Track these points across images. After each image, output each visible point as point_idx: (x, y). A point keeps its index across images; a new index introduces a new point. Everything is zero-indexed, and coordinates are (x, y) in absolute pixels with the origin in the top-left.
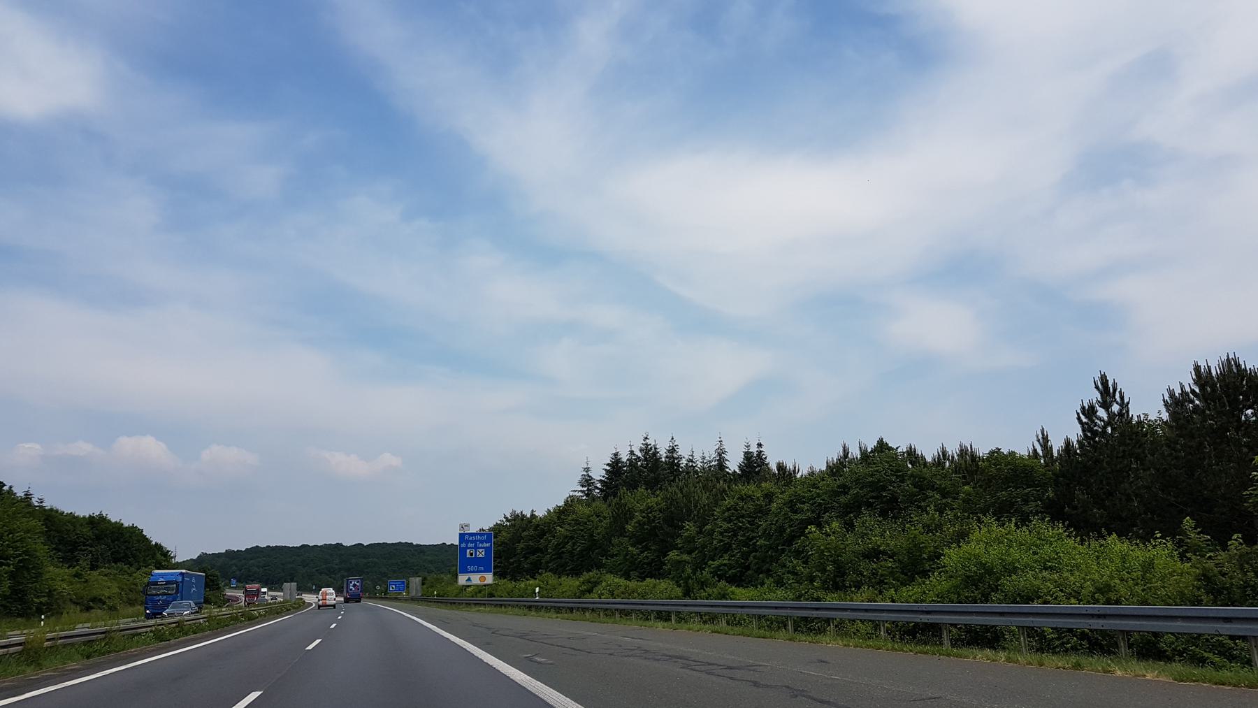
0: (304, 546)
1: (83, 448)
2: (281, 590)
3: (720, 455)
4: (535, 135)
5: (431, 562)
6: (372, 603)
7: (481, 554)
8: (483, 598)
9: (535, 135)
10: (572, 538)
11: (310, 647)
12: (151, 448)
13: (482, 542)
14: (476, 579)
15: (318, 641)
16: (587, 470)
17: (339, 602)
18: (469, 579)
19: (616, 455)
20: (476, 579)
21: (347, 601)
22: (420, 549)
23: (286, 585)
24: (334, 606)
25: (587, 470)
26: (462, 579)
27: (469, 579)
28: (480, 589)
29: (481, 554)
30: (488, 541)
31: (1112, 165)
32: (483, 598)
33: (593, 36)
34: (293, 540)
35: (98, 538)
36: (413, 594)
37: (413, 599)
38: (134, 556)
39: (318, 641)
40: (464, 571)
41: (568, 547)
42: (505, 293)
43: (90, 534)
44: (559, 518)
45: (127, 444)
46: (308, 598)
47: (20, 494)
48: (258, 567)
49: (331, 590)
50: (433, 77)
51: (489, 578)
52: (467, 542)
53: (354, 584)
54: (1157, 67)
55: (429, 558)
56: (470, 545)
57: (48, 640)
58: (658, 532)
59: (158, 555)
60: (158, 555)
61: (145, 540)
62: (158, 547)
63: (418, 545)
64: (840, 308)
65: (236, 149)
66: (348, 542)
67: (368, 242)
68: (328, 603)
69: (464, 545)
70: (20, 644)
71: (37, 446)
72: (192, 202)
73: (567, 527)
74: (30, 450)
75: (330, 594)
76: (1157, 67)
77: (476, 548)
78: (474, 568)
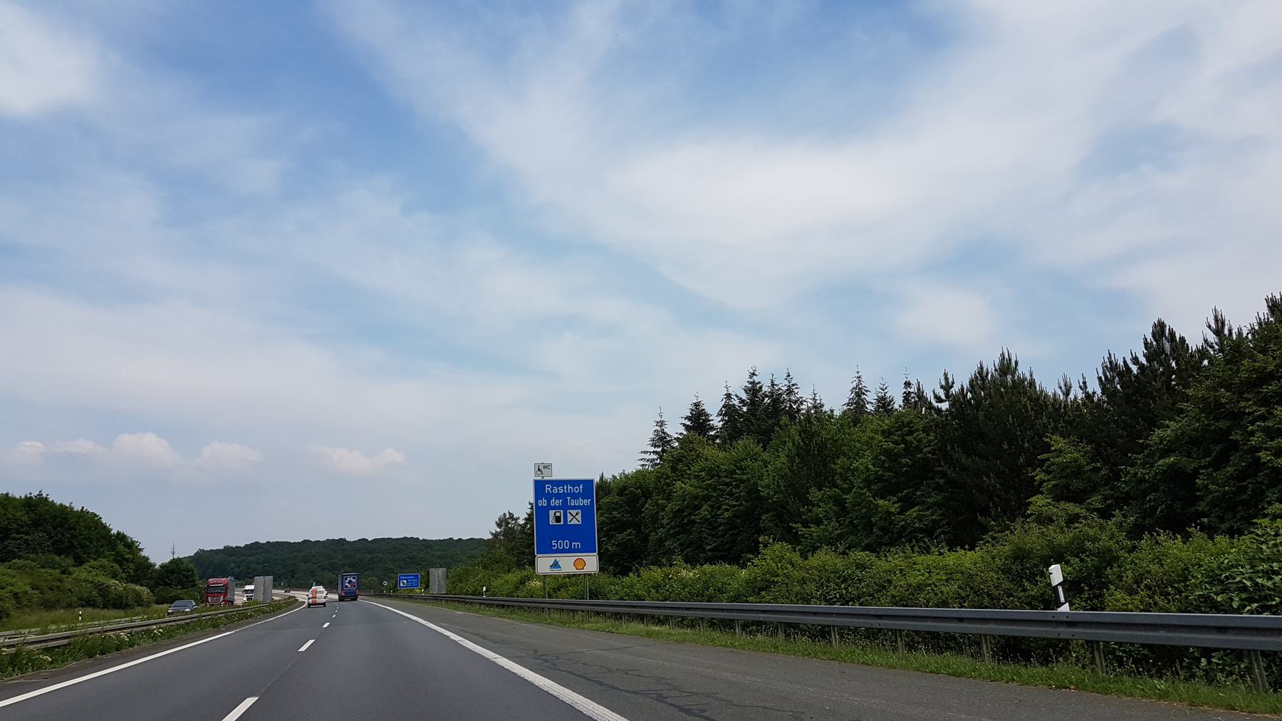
0: (305, 541)
1: (84, 446)
3: (858, 395)
4: (534, 125)
5: (439, 557)
6: (378, 604)
7: (575, 518)
8: (569, 600)
9: (534, 125)
10: (707, 498)
11: (303, 649)
12: (152, 445)
13: (575, 496)
14: (567, 564)
15: (311, 642)
16: (661, 424)
17: (332, 601)
18: (556, 565)
20: (567, 564)
21: (341, 599)
24: (324, 604)
25: (661, 424)
26: (544, 564)
27: (556, 565)
28: (561, 584)
29: (575, 518)
30: (584, 495)
31: (1130, 149)
32: (569, 600)
33: (593, 24)
34: (295, 536)
35: (36, 524)
36: (434, 589)
37: (436, 599)
39: (311, 642)
40: (547, 550)
41: (704, 511)
42: (505, 286)
43: (25, 518)
44: (674, 469)
45: (127, 442)
46: (302, 596)
48: (257, 563)
49: (321, 588)
50: (435, 71)
51: (591, 563)
52: (549, 497)
53: (350, 581)
54: (1179, 46)
55: (438, 553)
56: (554, 502)
57: (8, 647)
58: (742, 505)
59: (121, 547)
60: (121, 547)
61: (106, 529)
62: (121, 537)
63: (424, 540)
64: (851, 297)
65: (229, 140)
66: (352, 537)
67: (368, 236)
68: (318, 601)
70: (13, 646)
71: (39, 445)
73: (694, 481)
74: (31, 448)
75: (321, 592)
76: (1179, 46)
77: (565, 507)
78: (565, 544)
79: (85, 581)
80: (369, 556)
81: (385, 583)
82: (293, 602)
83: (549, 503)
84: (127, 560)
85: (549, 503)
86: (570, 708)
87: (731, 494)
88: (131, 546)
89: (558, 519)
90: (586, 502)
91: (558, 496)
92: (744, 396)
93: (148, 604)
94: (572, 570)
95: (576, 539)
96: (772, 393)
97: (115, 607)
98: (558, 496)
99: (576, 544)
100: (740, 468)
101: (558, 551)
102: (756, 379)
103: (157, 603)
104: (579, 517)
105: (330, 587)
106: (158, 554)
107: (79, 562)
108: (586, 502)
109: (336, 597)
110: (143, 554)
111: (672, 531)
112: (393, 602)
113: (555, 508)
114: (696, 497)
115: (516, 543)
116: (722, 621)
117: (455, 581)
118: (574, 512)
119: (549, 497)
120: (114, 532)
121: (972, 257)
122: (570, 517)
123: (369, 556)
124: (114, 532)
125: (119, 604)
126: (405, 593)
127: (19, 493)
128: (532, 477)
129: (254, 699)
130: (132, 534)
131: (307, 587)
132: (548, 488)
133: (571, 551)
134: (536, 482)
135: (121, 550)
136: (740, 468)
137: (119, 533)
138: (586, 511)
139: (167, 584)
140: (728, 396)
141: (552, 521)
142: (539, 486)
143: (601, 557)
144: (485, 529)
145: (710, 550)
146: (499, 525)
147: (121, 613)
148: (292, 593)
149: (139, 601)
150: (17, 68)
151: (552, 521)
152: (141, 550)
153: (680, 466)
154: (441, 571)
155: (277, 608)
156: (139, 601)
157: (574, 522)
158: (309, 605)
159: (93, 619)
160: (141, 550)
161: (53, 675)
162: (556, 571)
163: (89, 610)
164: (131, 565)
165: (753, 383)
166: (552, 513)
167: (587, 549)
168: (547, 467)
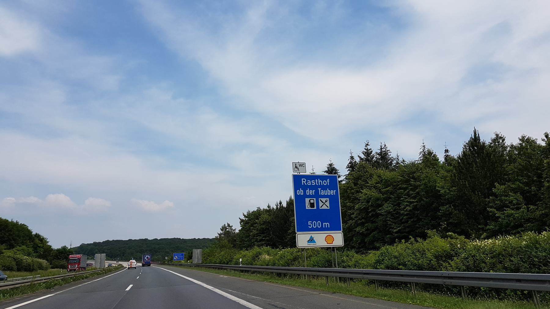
0: (130, 240)
1: (33, 199)
2: (93, 259)
6: (164, 269)
9: (230, 60)
12: (63, 199)
13: (324, 188)
14: (321, 239)
18: (311, 240)
19: (331, 165)
20: (321, 239)
21: (143, 265)
22: (184, 241)
23: (98, 256)
24: (135, 268)
26: (302, 240)
27: (311, 240)
31: (483, 73)
33: (255, 17)
37: (197, 266)
38: (14, 240)
40: (305, 228)
42: (218, 131)
44: (355, 184)
46: (125, 264)
47: (10, 220)
49: (134, 261)
50: (184, 35)
52: (305, 188)
53: (147, 257)
54: (503, 29)
55: (189, 245)
56: (309, 192)
60: (37, 241)
61: (30, 232)
62: (37, 236)
63: (183, 239)
65: (98, 67)
67: (157, 108)
68: (133, 266)
69: (301, 192)
71: (13, 199)
72: (80, 92)
74: (10, 200)
75: (134, 263)
76: (503, 29)
77: (317, 196)
78: (318, 224)
79: (9, 257)
80: (158, 246)
81: (166, 258)
82: (122, 267)
83: (305, 192)
84: (39, 247)
85: (305, 192)
86: (231, 300)
87: (408, 195)
88: (42, 240)
89: (312, 205)
90: (332, 192)
91: (311, 187)
92: (363, 156)
93: (46, 269)
94: (324, 244)
95: (327, 221)
96: (381, 153)
97: (26, 270)
98: (311, 187)
99: (326, 224)
100: (413, 178)
101: (313, 230)
102: (369, 147)
103: (52, 268)
104: (328, 204)
105: (138, 260)
106: (55, 244)
107: (11, 247)
108: (332, 192)
109: (141, 264)
110: (49, 244)
111: (359, 222)
112: (171, 267)
113: (309, 196)
114: (378, 199)
115: (270, 229)
116: (491, 289)
117: (205, 257)
118: (324, 200)
119: (305, 188)
120: (34, 233)
121: (416, 118)
122: (321, 204)
123: (158, 246)
124: (34, 233)
125: (29, 269)
126: (176, 263)
127: (4, 218)
128: (289, 174)
129: (132, 285)
130: (43, 234)
131: (128, 260)
132: (303, 181)
133: (322, 229)
134: (295, 177)
135: (37, 243)
136: (413, 178)
137: (36, 234)
138: (333, 199)
139: (59, 259)
140: (352, 158)
141: (308, 207)
142: (297, 180)
143: (345, 236)
144: (212, 232)
145: (396, 233)
146: (222, 230)
147: (28, 273)
148: (120, 263)
149: (41, 267)
150: (1, 35)
151: (308, 207)
152: (48, 242)
153: (360, 182)
154: (199, 250)
155: (110, 270)
156: (41, 267)
157: (324, 207)
158: (129, 268)
159: (14, 277)
160: (48, 242)
161: (19, 300)
162: (312, 245)
163: (8, 272)
164: (42, 249)
165: (367, 150)
166: (307, 200)
167: (334, 227)
168: (302, 165)
